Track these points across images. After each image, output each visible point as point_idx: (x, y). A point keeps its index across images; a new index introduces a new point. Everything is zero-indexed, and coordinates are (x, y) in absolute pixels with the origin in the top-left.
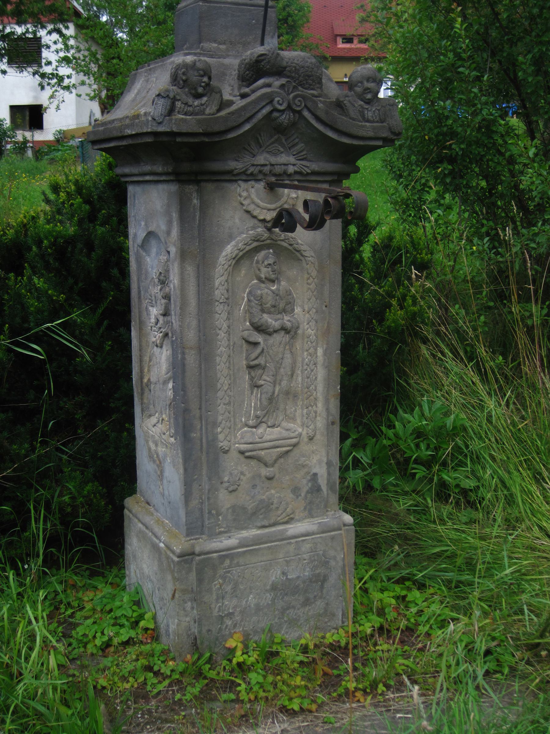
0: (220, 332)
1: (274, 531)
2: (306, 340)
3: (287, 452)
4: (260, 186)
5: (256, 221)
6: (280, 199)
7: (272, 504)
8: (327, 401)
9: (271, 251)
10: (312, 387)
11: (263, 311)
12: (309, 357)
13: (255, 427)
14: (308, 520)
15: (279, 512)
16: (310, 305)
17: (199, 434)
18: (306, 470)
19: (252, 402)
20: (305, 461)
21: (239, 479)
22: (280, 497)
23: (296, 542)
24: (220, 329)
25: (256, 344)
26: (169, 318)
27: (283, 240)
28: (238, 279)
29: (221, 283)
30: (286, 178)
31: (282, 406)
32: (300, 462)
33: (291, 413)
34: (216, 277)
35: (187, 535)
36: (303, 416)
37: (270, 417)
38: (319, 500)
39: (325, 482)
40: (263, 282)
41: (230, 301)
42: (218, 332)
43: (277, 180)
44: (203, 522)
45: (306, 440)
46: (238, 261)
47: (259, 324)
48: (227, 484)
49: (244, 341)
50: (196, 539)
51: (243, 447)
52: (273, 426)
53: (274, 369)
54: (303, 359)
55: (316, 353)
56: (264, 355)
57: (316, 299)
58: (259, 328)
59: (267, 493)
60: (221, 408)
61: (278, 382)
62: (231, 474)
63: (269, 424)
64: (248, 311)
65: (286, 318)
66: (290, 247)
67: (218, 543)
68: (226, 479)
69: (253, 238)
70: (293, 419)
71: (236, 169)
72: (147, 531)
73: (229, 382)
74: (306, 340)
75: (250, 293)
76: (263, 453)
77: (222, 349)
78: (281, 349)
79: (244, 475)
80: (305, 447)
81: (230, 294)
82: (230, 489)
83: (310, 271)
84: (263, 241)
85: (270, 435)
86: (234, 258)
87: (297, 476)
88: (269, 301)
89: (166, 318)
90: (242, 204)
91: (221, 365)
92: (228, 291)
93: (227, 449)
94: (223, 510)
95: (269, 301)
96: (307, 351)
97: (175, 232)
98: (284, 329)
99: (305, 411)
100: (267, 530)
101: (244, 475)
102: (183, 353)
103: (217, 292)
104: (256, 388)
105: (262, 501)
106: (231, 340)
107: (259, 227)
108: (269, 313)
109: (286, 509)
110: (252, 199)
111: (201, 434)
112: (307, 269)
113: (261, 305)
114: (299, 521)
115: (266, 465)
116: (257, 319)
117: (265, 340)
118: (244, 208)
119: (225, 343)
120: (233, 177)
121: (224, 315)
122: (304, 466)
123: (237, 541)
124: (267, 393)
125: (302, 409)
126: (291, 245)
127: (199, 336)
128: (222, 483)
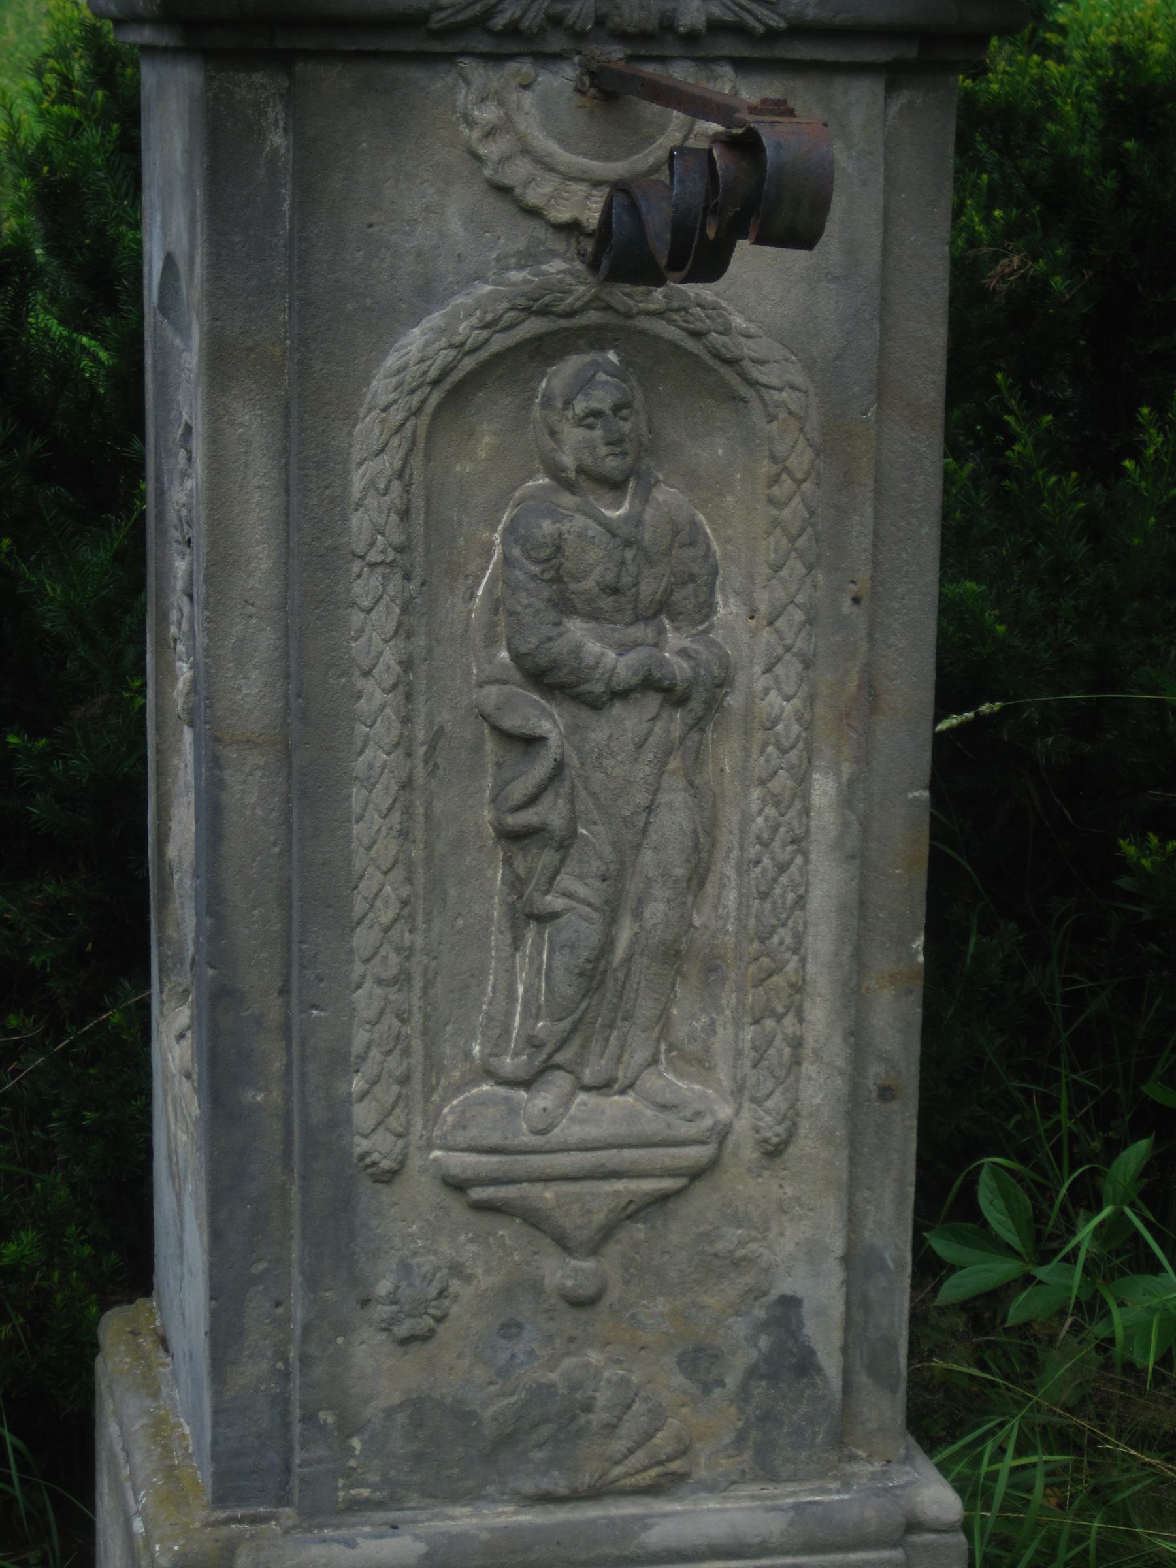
0: (369, 685)
1: (593, 1522)
2: (759, 736)
3: (664, 1198)
4: (560, 80)
5: (541, 233)
6: (649, 140)
7: (588, 1407)
8: (854, 1002)
9: (612, 356)
10: (784, 935)
11: (564, 606)
12: (770, 811)
13: (526, 1084)
14: (754, 1489)
15: (618, 1446)
16: (780, 594)
17: (276, 1095)
18: (748, 1280)
19: (519, 984)
20: (741, 1244)
21: (442, 1293)
22: (624, 1382)
24: (367, 674)
25: (531, 742)
27: (658, 314)
28: (463, 468)
29: (373, 482)
30: (674, 50)
31: (646, 1008)
32: (719, 1246)
33: (692, 1038)
34: (356, 457)
35: (220, 1500)
36: (739, 1054)
37: (595, 1047)
38: (803, 1409)
39: (837, 1337)
40: (569, 486)
41: (424, 555)
42: (360, 683)
44: (288, 1451)
45: (750, 1153)
46: (457, 392)
47: (543, 661)
48: (383, 1311)
49: (486, 726)
50: (253, 1520)
52: (604, 1087)
53: (607, 850)
54: (746, 819)
55: (806, 797)
56: (565, 789)
57: (810, 568)
58: (547, 678)
59: (568, 1363)
60: (367, 999)
61: (630, 904)
62: (405, 1269)
63: (588, 1075)
65: (675, 639)
67: (337, 1549)
68: (384, 1287)
69: (522, 302)
70: (698, 1062)
71: (441, 9)
73: (405, 891)
74: (759, 736)
75: (511, 529)
76: (549, 1194)
77: (375, 755)
78: (644, 770)
79: (468, 1279)
80: (743, 1184)
81: (419, 529)
82: (402, 1330)
83: (781, 449)
84: (570, 314)
85: (582, 1122)
86: (435, 383)
87: (706, 1299)
88: (593, 566)
90: (476, 157)
91: (371, 825)
92: (405, 514)
93: (386, 1164)
95: (593, 566)
96: (762, 782)
98: (654, 685)
99: (749, 1033)
101: (468, 1279)
104: (533, 925)
105: (542, 1392)
106: (421, 719)
107: (553, 254)
108: (594, 616)
109: (649, 1436)
110: (521, 138)
111: (287, 1098)
113: (558, 579)
114: (712, 1488)
115: (563, 1243)
116: (534, 640)
117: (574, 729)
118: (487, 172)
119: (386, 729)
121: (386, 618)
122: (738, 1264)
123: (421, 1548)
124: (573, 948)
125: (738, 1026)
126: (697, 335)
127: (286, 697)
128: (365, 1302)
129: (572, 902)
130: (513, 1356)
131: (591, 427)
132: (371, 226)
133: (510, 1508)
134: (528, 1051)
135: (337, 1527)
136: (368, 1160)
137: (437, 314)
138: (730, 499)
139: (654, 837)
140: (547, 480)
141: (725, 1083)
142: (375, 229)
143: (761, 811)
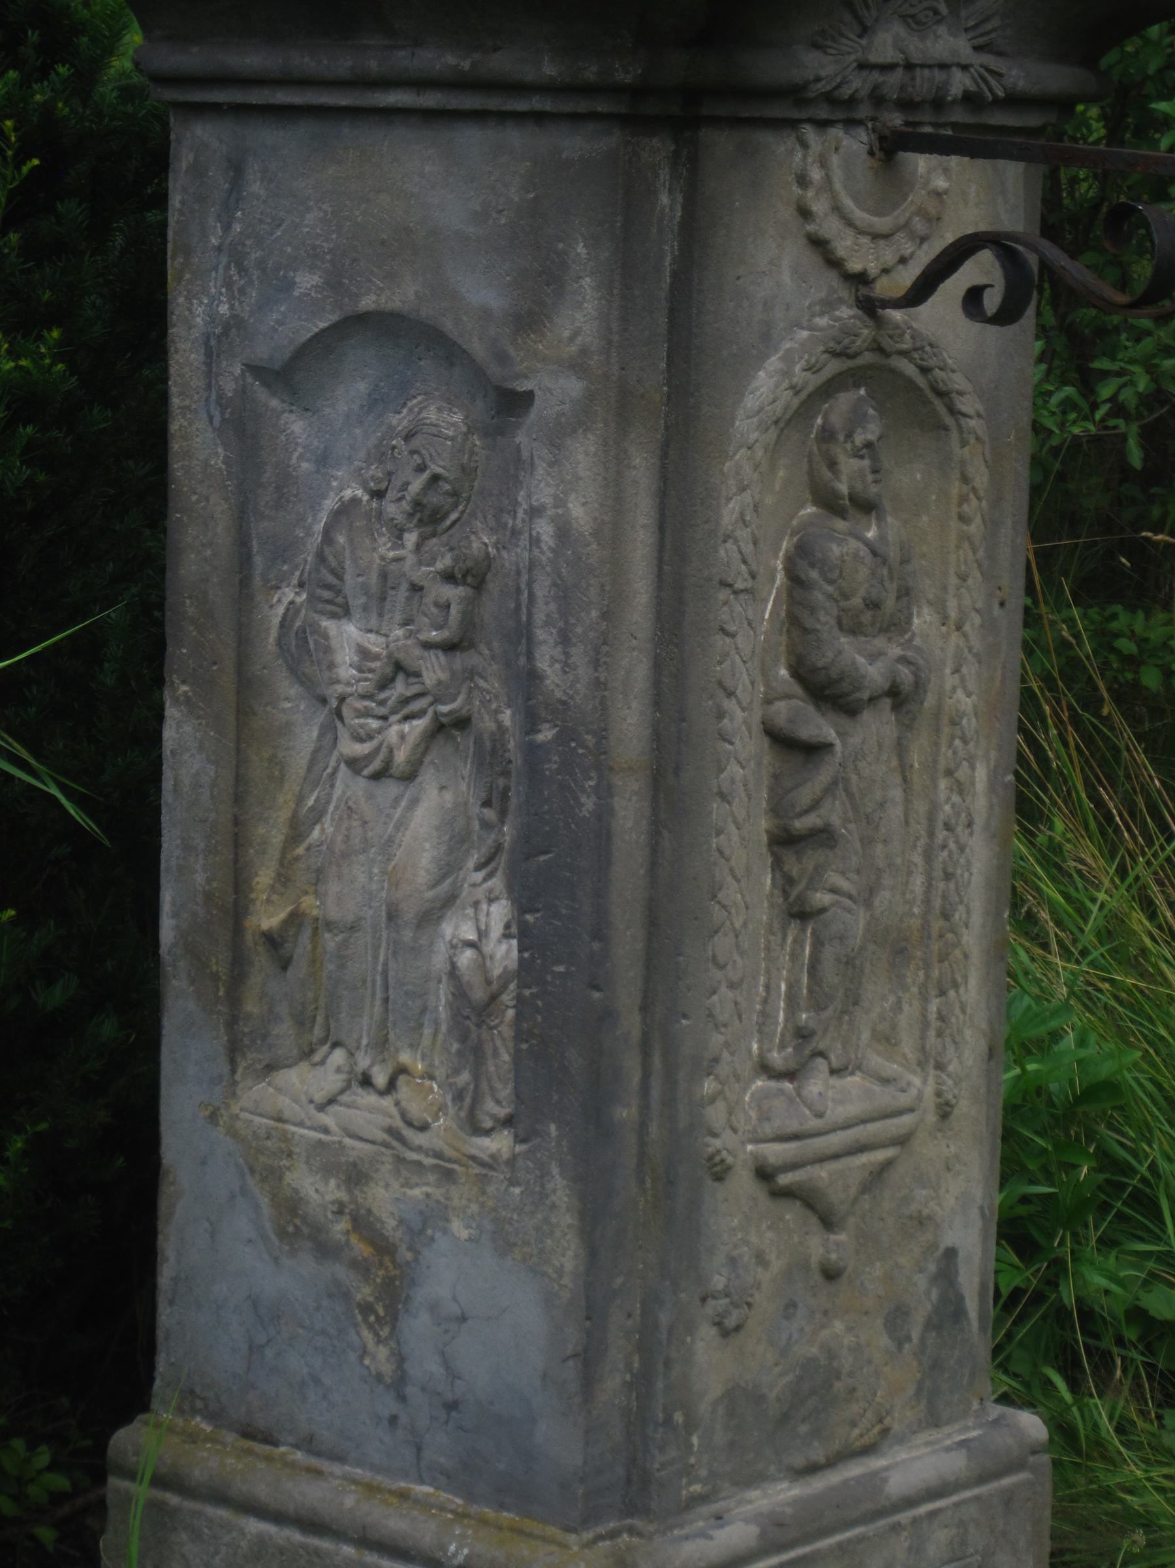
1: (845, 1482)
2: (946, 730)
4: (852, 146)
7: (838, 1378)
12: (956, 798)
14: (924, 1437)
23: (915, 1521)
25: (813, 751)
26: (472, 659)
36: (925, 1024)
40: (841, 513)
43: (907, 123)
45: (931, 1118)
51: (775, 1152)
54: (934, 809)
64: (796, 621)
66: (921, 381)
67: (701, 1542)
71: (818, 79)
72: (325, 1544)
76: (822, 1173)
80: (932, 1149)
85: (842, 1102)
89: (459, 660)
94: (704, 1408)
96: (949, 773)
97: (581, 317)
99: (933, 1008)
100: (818, 1484)
102: (605, 792)
103: (726, 552)
107: (841, 301)
112: (963, 463)
114: (901, 1440)
118: (811, 228)
120: (795, 107)
125: (925, 999)
126: (925, 370)
128: (704, 1300)
129: (836, 897)
130: (791, 1336)
131: (862, 457)
132: (738, 278)
133: (785, 1485)
134: (795, 1042)
135: (681, 1526)
136: (717, 1159)
137: (773, 358)
138: (925, 519)
139: (883, 830)
140: (814, 509)
141: (910, 1056)
142: (742, 281)
143: (949, 799)
